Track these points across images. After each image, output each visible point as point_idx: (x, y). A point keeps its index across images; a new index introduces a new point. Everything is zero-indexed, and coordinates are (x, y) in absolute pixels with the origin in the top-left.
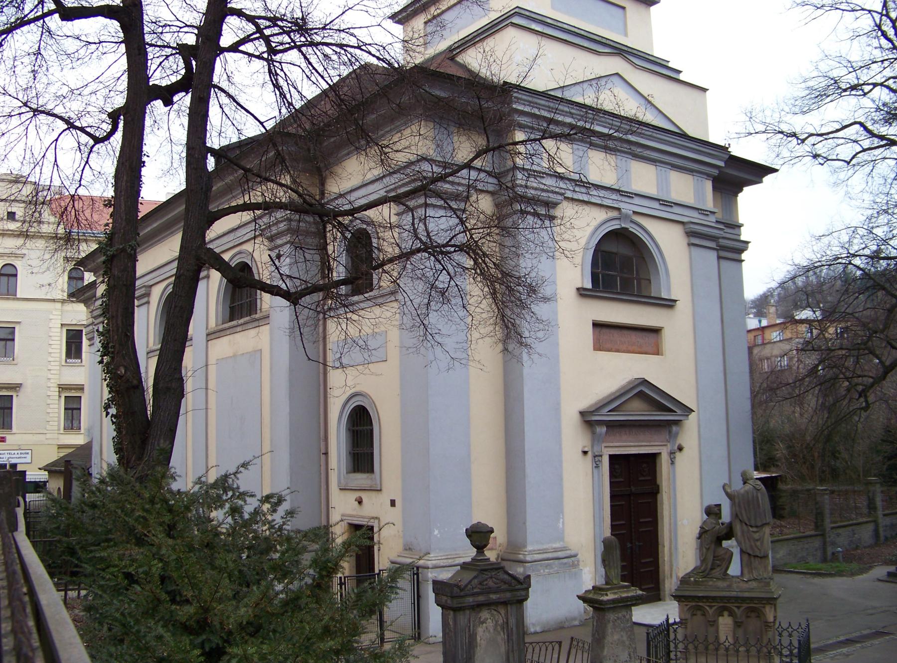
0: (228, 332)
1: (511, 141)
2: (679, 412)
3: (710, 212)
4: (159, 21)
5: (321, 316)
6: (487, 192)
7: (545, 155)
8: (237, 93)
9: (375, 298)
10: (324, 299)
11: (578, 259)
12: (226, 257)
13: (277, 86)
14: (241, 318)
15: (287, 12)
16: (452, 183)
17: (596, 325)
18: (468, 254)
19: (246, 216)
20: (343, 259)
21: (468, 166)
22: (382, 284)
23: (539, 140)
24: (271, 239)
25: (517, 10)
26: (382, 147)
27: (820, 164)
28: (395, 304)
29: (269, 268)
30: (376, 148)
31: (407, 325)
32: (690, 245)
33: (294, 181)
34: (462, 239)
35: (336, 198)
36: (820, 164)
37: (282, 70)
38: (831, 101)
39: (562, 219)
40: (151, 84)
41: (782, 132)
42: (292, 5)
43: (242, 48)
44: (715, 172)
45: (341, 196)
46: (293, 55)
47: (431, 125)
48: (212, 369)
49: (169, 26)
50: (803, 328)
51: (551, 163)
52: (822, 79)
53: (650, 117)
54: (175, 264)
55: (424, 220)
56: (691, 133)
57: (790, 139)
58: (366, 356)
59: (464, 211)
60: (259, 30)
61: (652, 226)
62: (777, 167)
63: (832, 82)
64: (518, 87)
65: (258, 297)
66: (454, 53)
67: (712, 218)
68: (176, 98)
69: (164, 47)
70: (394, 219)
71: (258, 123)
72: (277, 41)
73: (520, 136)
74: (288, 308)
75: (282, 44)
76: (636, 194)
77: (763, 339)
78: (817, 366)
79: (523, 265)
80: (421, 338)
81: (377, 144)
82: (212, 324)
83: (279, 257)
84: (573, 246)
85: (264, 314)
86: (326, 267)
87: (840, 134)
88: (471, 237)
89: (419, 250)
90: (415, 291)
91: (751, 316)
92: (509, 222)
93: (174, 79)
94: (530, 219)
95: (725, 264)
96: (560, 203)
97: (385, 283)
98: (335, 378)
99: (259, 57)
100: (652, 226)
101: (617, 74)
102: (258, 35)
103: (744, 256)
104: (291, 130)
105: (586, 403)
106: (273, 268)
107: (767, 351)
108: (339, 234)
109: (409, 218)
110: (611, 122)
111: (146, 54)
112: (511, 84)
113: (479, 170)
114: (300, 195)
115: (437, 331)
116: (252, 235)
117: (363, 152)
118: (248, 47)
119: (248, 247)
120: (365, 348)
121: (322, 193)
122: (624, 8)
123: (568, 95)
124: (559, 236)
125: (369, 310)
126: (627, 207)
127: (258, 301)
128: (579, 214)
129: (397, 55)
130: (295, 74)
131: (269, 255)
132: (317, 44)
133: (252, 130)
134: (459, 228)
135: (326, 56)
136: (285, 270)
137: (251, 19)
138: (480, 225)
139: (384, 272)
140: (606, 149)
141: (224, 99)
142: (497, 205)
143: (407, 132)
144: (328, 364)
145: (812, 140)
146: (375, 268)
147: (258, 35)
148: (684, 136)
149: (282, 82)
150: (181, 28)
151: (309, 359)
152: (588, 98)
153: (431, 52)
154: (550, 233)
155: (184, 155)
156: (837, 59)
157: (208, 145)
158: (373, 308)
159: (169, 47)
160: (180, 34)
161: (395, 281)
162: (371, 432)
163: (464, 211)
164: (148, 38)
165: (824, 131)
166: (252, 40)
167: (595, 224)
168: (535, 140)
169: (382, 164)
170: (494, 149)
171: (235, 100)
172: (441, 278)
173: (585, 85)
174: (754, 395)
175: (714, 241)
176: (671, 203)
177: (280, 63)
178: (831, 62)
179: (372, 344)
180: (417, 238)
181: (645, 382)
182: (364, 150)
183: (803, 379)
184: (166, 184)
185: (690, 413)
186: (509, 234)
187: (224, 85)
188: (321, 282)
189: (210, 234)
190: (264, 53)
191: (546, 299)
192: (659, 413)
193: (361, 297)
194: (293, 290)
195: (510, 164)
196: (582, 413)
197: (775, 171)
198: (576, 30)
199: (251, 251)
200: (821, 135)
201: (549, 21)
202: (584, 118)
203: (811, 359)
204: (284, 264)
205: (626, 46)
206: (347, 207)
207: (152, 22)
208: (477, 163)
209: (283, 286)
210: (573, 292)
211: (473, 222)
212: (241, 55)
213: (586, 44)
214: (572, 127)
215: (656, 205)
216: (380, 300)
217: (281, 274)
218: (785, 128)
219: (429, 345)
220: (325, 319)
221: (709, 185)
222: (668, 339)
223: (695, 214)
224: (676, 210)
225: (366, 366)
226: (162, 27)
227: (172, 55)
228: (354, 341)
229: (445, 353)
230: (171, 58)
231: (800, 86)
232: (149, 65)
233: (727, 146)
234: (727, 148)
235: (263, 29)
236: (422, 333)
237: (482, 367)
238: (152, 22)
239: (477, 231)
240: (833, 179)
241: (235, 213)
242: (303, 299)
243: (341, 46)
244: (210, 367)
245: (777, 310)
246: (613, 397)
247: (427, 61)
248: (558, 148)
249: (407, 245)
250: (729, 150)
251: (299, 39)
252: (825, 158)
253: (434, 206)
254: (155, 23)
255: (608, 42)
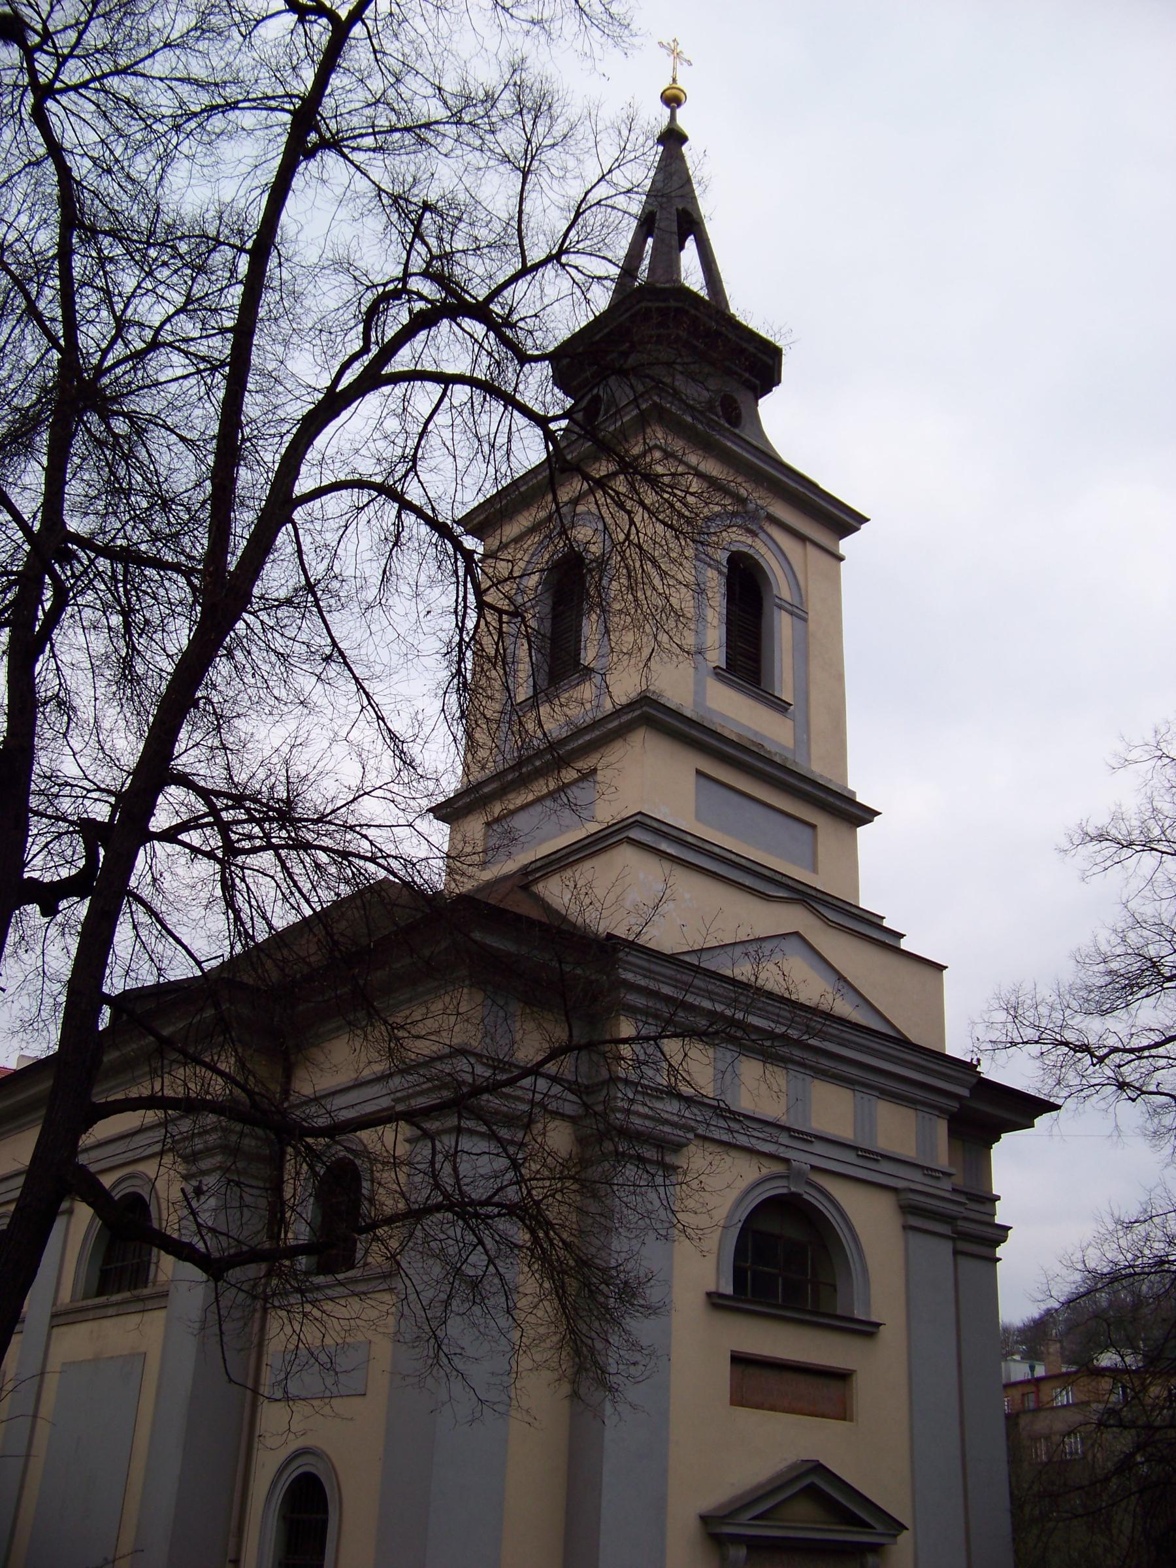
0: (91, 1315)
1: (608, 1037)
2: (880, 1528)
3: (943, 1173)
4: (57, 777)
5: (259, 1304)
6: (563, 1116)
7: (665, 1065)
8: (164, 908)
9: (354, 1281)
10: (269, 1274)
11: (712, 1242)
12: (107, 1181)
13: (230, 903)
14: (119, 1291)
15: (264, 789)
16: (507, 1096)
17: (738, 1360)
18: (522, 1220)
19: (151, 1116)
20: (309, 1209)
21: (534, 1071)
22: (370, 1260)
23: (655, 1039)
24: (191, 1158)
25: (638, 818)
26: (393, 1028)
27: (1130, 1098)
28: (386, 1297)
29: (179, 1212)
30: (383, 1028)
31: (407, 1336)
32: (906, 1228)
33: (241, 1062)
34: (512, 1194)
35: (305, 1103)
36: (1130, 1098)
37: (243, 880)
38: (1148, 996)
39: (685, 1174)
40: (26, 876)
41: (1066, 1044)
42: (273, 779)
43: (184, 837)
44: (954, 1105)
45: (316, 1100)
46: (266, 859)
47: (479, 997)
48: (52, 1382)
49: (72, 786)
50: (1106, 1384)
51: (673, 1079)
52: (1132, 960)
53: (844, 1008)
54: (21, 1180)
55: (453, 1156)
56: (914, 1036)
57: (1079, 1055)
58: (329, 1381)
59: (522, 1145)
60: (214, 811)
61: (841, 1192)
62: (1059, 1102)
63: (1149, 964)
64: (632, 945)
65: (154, 1260)
66: (531, 878)
67: (946, 1184)
68: (63, 904)
69: (58, 819)
70: (402, 1150)
71: (193, 963)
72: (241, 831)
73: (627, 1029)
74: (203, 1285)
75: (250, 837)
76: (816, 1137)
77: (1038, 1401)
78: (1132, 1455)
79: (615, 1245)
80: (430, 1361)
81: (386, 1022)
82: (65, 1296)
83: (198, 1192)
84: (702, 1221)
85: (161, 1289)
86: (277, 1220)
87: (1161, 1051)
88: (529, 1193)
89: (438, 1208)
90: (425, 1278)
91: (1017, 1357)
92: (594, 1173)
93: (65, 873)
94: (630, 1171)
95: (966, 1264)
96: (686, 1145)
97: (376, 1258)
98: (272, 1417)
99: (210, 855)
100: (841, 1192)
101: (797, 934)
102: (211, 819)
103: (1000, 1251)
104: (248, 979)
105: (711, 1499)
106: (186, 1212)
107: (1042, 1424)
108: (305, 1166)
109: (427, 1152)
110: (777, 1011)
111: (26, 829)
112: (619, 938)
113: (554, 1079)
114: (250, 1093)
115: (458, 1351)
116: (157, 1148)
117: (359, 1032)
118: (193, 837)
119: (149, 1169)
120: (330, 1367)
121: (286, 1092)
122: (813, 827)
123: (708, 963)
124: (678, 1203)
125: (342, 1302)
126: (801, 1158)
127: (153, 1267)
128: (714, 1167)
129: (434, 875)
130: (265, 890)
131: (183, 1190)
132: (307, 846)
133: (180, 970)
134: (510, 1175)
135: (318, 866)
136: (206, 1218)
137: (203, 793)
138: (546, 1173)
139: (377, 1239)
140: (768, 1057)
141: (142, 917)
142: (581, 1141)
143: (437, 1007)
144: (261, 1392)
145: (1116, 1058)
146: (362, 1231)
147: (211, 819)
148: (903, 1042)
149: (240, 901)
150: (89, 791)
151: (231, 1380)
152: (743, 971)
153: (487, 875)
154: (663, 1196)
155: (63, 999)
156: (1155, 929)
157: (105, 990)
158: (350, 1299)
159: (65, 820)
160: (87, 802)
161: (393, 1256)
162: (325, 1523)
163: (522, 1145)
164: (34, 802)
165: (1135, 1043)
166: (202, 826)
167: (742, 1185)
168: (647, 1039)
169: (391, 1056)
170: (579, 1048)
171: (160, 921)
172: (472, 1259)
173: (739, 950)
174: (1017, 1503)
175: (947, 1223)
176: (877, 1154)
177: (242, 868)
178: (1145, 933)
179: (342, 1362)
180: (437, 1186)
181: (818, 1468)
182: (362, 1029)
183: (1107, 1479)
184: (24, 1045)
185: (900, 1532)
186: (595, 1195)
187: (146, 892)
188: (267, 1246)
189: (86, 1140)
190: (218, 848)
191: (651, 1310)
192: (843, 1528)
193: (329, 1279)
194: (216, 1255)
195: (605, 1074)
196: (705, 1519)
197: (1057, 1107)
198: (733, 857)
199: (153, 1176)
200: (1131, 1051)
201: (690, 839)
202: (733, 1003)
203: (1121, 1442)
204: (205, 1206)
205: (815, 889)
206: (322, 1122)
207: (45, 777)
208: (551, 1068)
209: (201, 1246)
210: (701, 1298)
211: (535, 1167)
212: (178, 848)
213: (748, 881)
214: (712, 1015)
215: (850, 1157)
216: (361, 1288)
217: (199, 1225)
218: (1070, 1036)
219: (442, 1373)
220: (265, 1310)
221: (942, 1127)
222: (864, 1390)
223: (917, 1176)
224: (885, 1166)
225: (327, 1400)
226: (59, 785)
227: (66, 833)
228: (312, 1354)
229: (467, 1389)
230: (66, 839)
231: (1096, 968)
232: (28, 845)
233: (975, 1062)
234: (976, 1066)
235: (222, 810)
236: (431, 1354)
237: (531, 1420)
238: (45, 777)
239: (540, 1184)
240: (1151, 1127)
241: (134, 1110)
242: (231, 1272)
243: (345, 855)
244: (47, 1377)
245: (1062, 1347)
246: (761, 1492)
247: (479, 889)
248: (686, 1055)
249: (422, 1194)
250: (978, 1069)
251: (279, 836)
252: (1137, 1089)
253: (472, 1132)
254: (49, 778)
255: (784, 880)
